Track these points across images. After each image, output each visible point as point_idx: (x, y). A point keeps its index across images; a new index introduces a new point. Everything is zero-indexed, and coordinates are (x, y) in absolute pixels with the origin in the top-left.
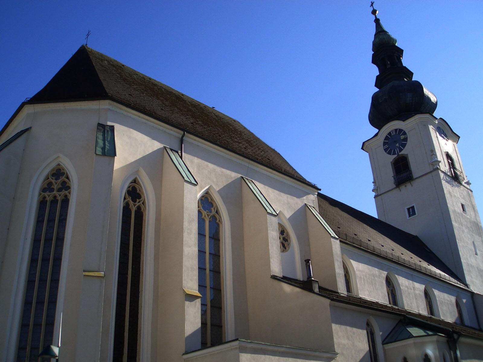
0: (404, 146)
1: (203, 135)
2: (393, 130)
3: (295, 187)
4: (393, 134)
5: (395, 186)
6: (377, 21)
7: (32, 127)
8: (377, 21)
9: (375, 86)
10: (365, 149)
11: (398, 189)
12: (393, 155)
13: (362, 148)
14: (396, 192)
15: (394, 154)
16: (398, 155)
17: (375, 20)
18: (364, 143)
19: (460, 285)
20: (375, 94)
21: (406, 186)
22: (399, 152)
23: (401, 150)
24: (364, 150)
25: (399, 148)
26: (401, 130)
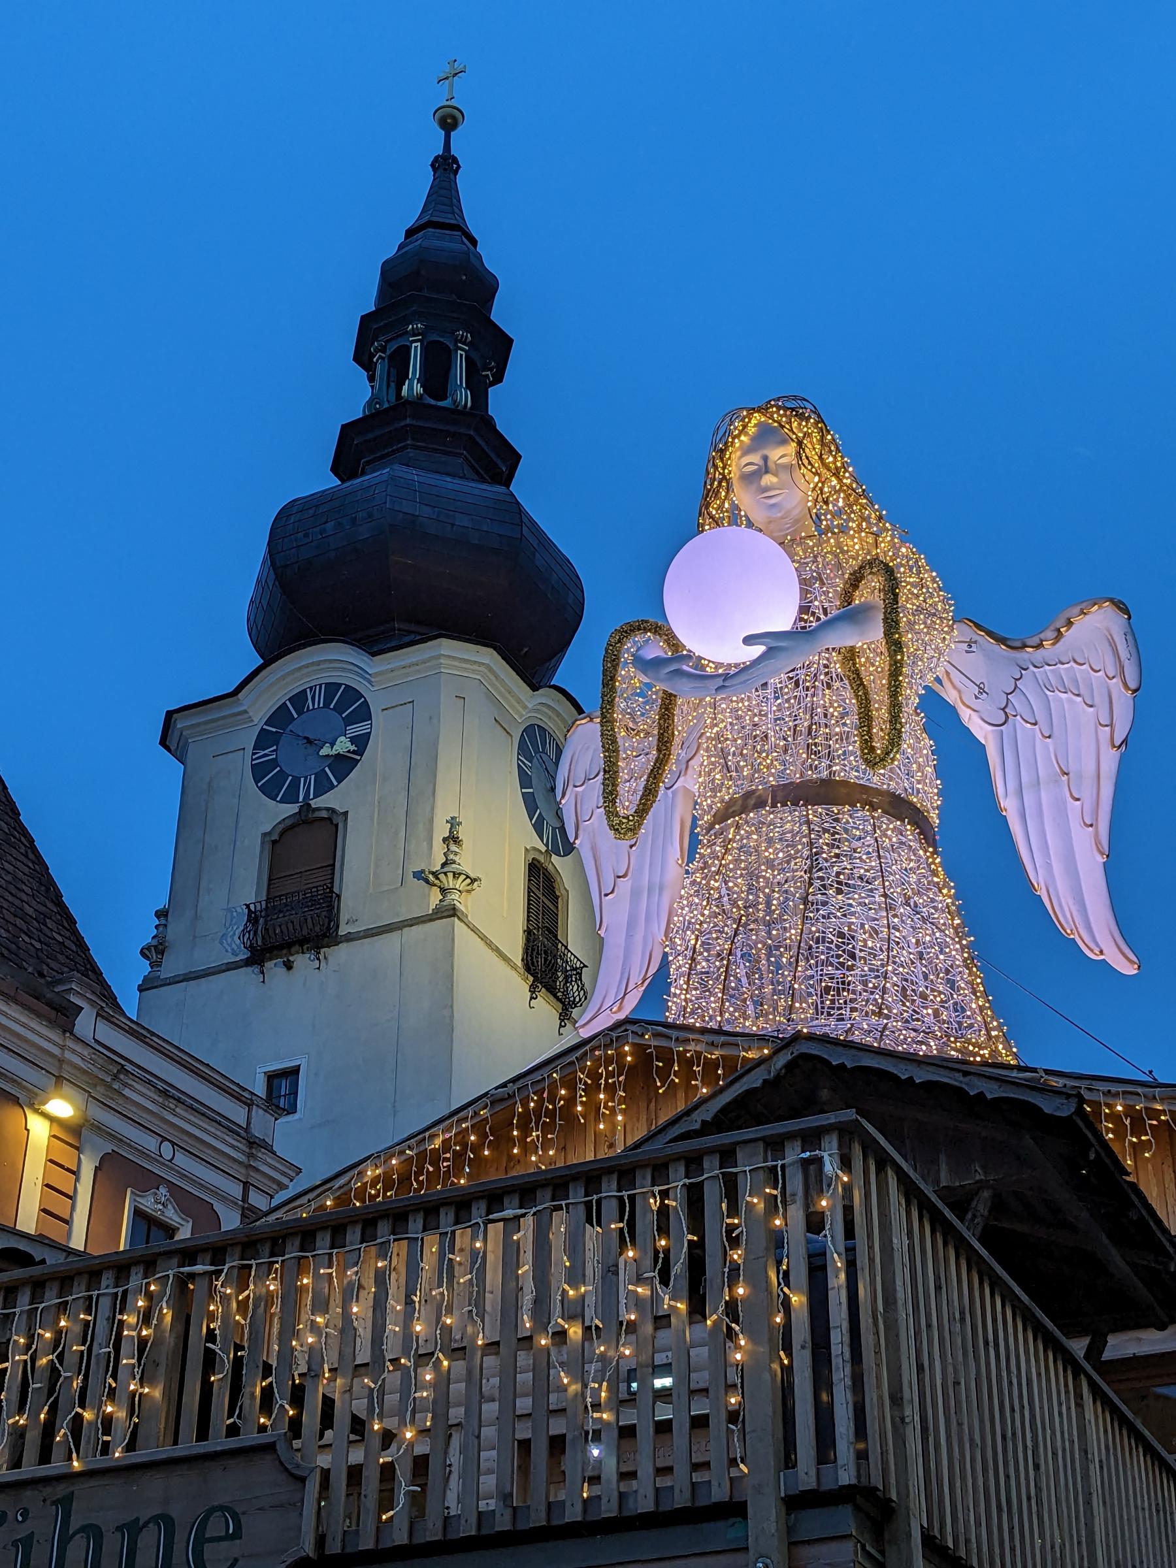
0: (344, 765)
1: (706, 863)
2: (321, 685)
4: (313, 704)
6: (446, 165)
8: (446, 165)
9: (520, 457)
10: (173, 748)
11: (256, 969)
13: (163, 742)
14: (247, 975)
18: (169, 714)
20: (285, 513)
21: (289, 966)
22: (311, 797)
23: (323, 787)
24: (169, 750)
25: (321, 777)
26: (352, 694)
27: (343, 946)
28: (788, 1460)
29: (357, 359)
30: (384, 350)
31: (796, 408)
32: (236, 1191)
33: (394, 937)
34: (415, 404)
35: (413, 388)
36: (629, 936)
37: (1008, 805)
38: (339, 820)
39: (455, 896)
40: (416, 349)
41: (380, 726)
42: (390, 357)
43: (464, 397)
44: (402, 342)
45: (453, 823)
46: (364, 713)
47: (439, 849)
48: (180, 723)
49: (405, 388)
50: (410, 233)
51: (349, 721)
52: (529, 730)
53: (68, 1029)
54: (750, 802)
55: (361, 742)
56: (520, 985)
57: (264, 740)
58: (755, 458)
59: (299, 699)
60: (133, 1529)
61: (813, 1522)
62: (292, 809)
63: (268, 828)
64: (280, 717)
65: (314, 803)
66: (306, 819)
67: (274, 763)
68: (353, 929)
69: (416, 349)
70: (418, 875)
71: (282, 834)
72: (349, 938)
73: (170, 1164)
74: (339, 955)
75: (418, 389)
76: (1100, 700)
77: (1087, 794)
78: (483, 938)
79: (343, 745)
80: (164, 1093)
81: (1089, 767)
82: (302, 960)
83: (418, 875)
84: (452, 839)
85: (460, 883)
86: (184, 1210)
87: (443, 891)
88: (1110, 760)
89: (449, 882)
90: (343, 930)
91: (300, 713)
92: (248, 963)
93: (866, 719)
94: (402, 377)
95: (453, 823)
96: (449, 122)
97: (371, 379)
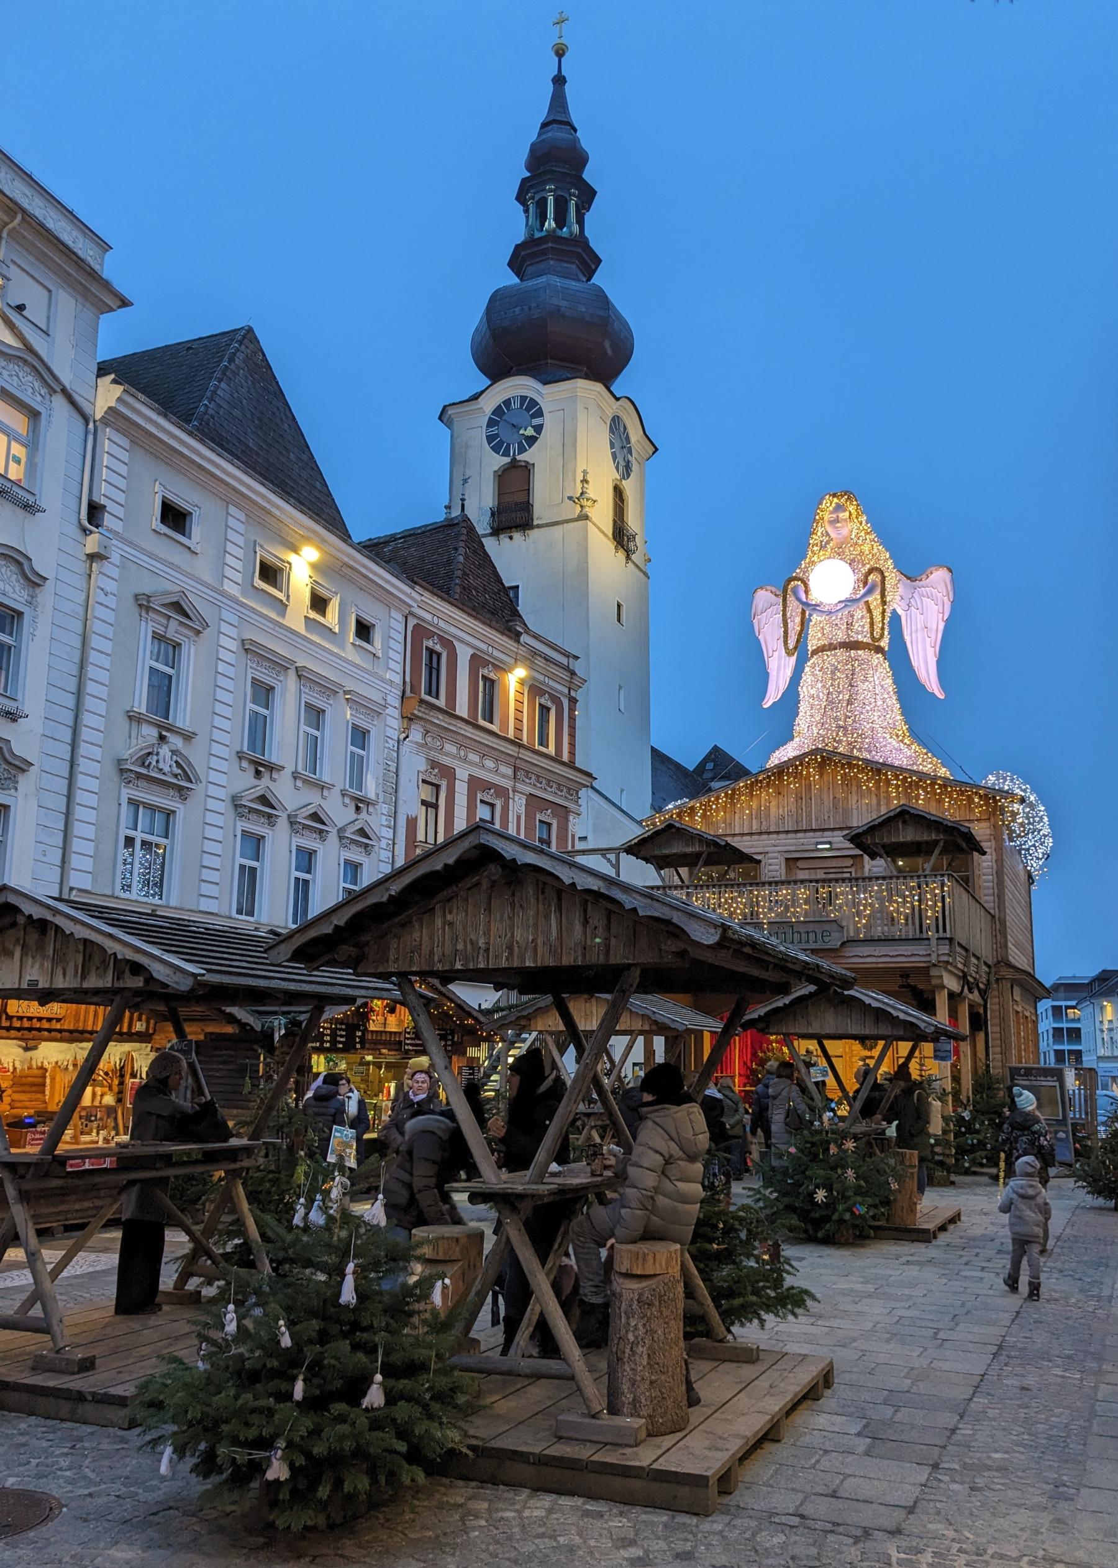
0: (532, 440)
3: (650, 1018)
5: (489, 531)
6: (559, 81)
7: (170, 497)
8: (559, 81)
12: (503, 455)
13: (440, 418)
15: (506, 454)
16: (514, 459)
17: (555, 77)
18: (445, 407)
19: (185, 710)
21: (511, 538)
23: (522, 450)
25: (520, 444)
26: (533, 403)
27: (536, 530)
28: (938, 931)
29: (518, 199)
30: (532, 198)
31: (849, 494)
32: (566, 691)
33: (559, 528)
34: (551, 236)
35: (550, 224)
36: (778, 673)
37: (907, 638)
38: (530, 467)
39: (587, 509)
40: (551, 199)
41: (548, 420)
42: (537, 202)
43: (576, 228)
44: (543, 194)
45: (585, 472)
46: (540, 413)
47: (579, 485)
48: (450, 411)
49: (547, 224)
50: (544, 125)
51: (533, 416)
52: (613, 419)
53: (518, 642)
54: (831, 647)
55: (539, 429)
56: (610, 545)
57: (491, 423)
58: (834, 516)
59: (507, 402)
60: (808, 933)
61: (941, 942)
62: (507, 460)
63: (496, 468)
64: (498, 411)
65: (518, 458)
66: (514, 465)
67: (497, 436)
68: (540, 522)
69: (551, 199)
70: (570, 498)
71: (504, 471)
72: (539, 526)
73: (548, 685)
74: (534, 534)
75: (553, 224)
76: (940, 602)
77: (933, 636)
78: (598, 528)
79: (530, 432)
80: (547, 660)
81: (935, 627)
82: (517, 536)
83: (570, 498)
84: (585, 481)
85: (589, 503)
86: (553, 702)
87: (581, 506)
88: (942, 626)
89: (585, 503)
90: (536, 522)
91: (508, 410)
92: (491, 535)
93: (872, 624)
94: (543, 217)
95: (585, 472)
96: (560, 53)
97: (526, 211)
